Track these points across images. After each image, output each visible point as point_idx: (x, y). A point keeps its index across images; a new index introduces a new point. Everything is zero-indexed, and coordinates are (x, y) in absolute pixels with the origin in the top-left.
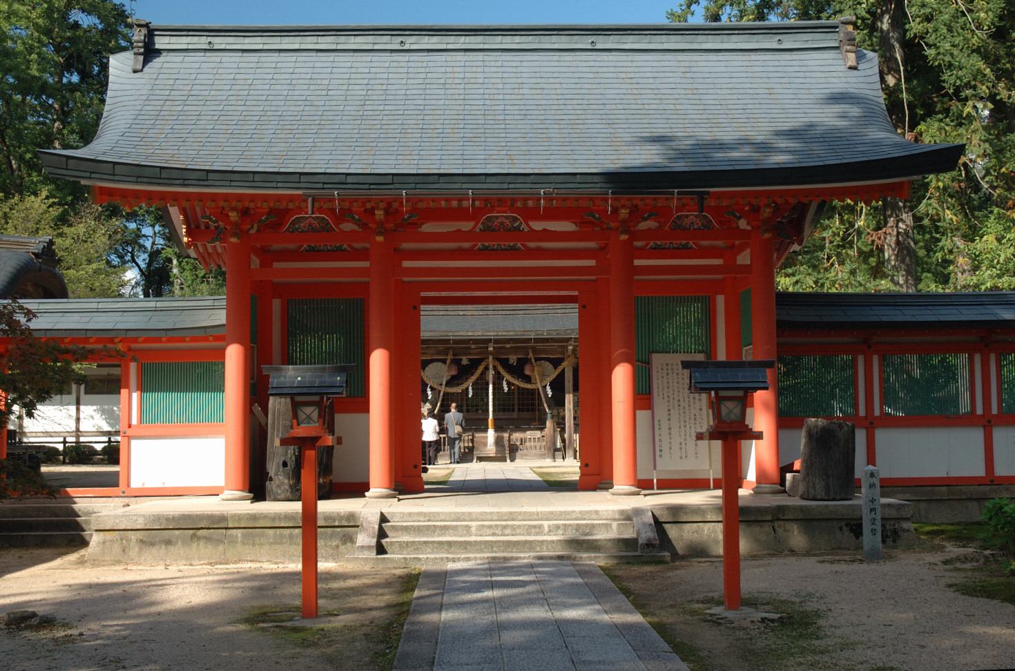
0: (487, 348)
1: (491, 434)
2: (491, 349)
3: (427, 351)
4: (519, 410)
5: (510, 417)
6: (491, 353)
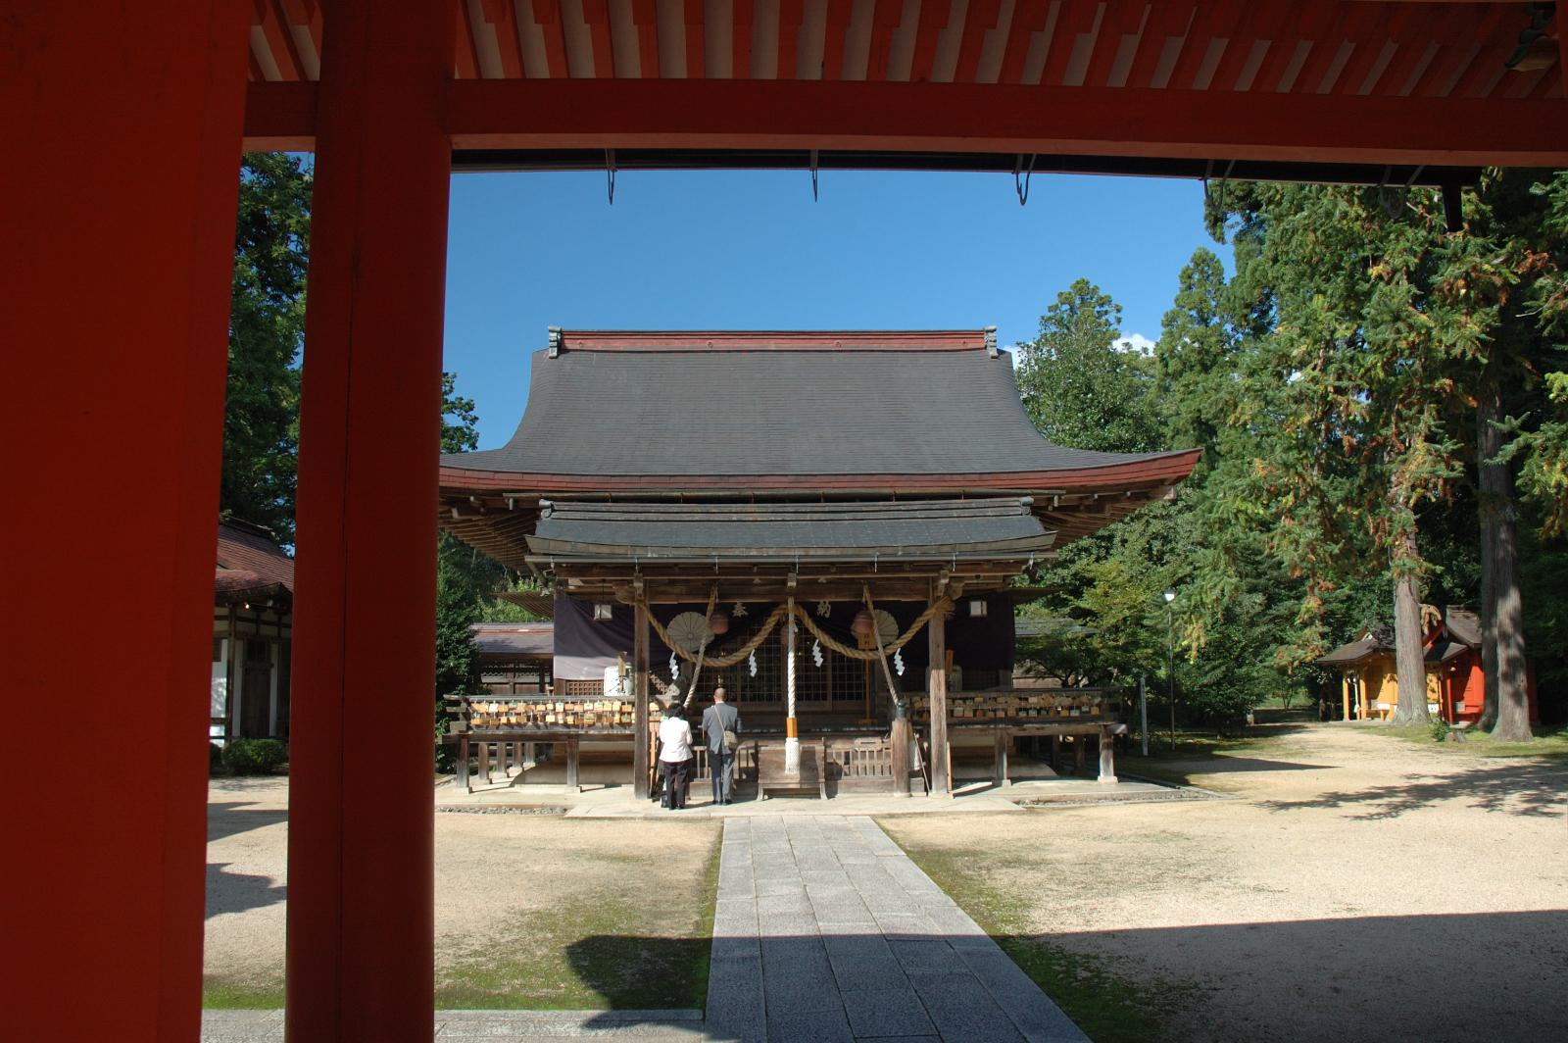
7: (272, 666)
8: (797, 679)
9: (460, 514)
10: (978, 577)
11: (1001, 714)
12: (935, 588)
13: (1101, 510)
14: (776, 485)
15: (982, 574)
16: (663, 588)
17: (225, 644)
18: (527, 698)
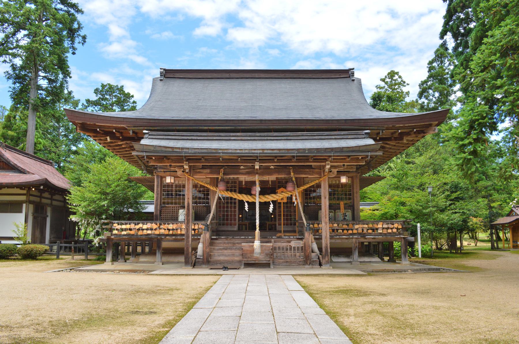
0: (253, 167)
1: (257, 244)
2: (257, 167)
7: (47, 216)
8: (255, 219)
9: (111, 139)
10: (344, 165)
11: (355, 231)
12: (324, 171)
13: (402, 139)
14: (251, 125)
15: (345, 164)
16: (199, 170)
17: (24, 205)
18: (135, 222)
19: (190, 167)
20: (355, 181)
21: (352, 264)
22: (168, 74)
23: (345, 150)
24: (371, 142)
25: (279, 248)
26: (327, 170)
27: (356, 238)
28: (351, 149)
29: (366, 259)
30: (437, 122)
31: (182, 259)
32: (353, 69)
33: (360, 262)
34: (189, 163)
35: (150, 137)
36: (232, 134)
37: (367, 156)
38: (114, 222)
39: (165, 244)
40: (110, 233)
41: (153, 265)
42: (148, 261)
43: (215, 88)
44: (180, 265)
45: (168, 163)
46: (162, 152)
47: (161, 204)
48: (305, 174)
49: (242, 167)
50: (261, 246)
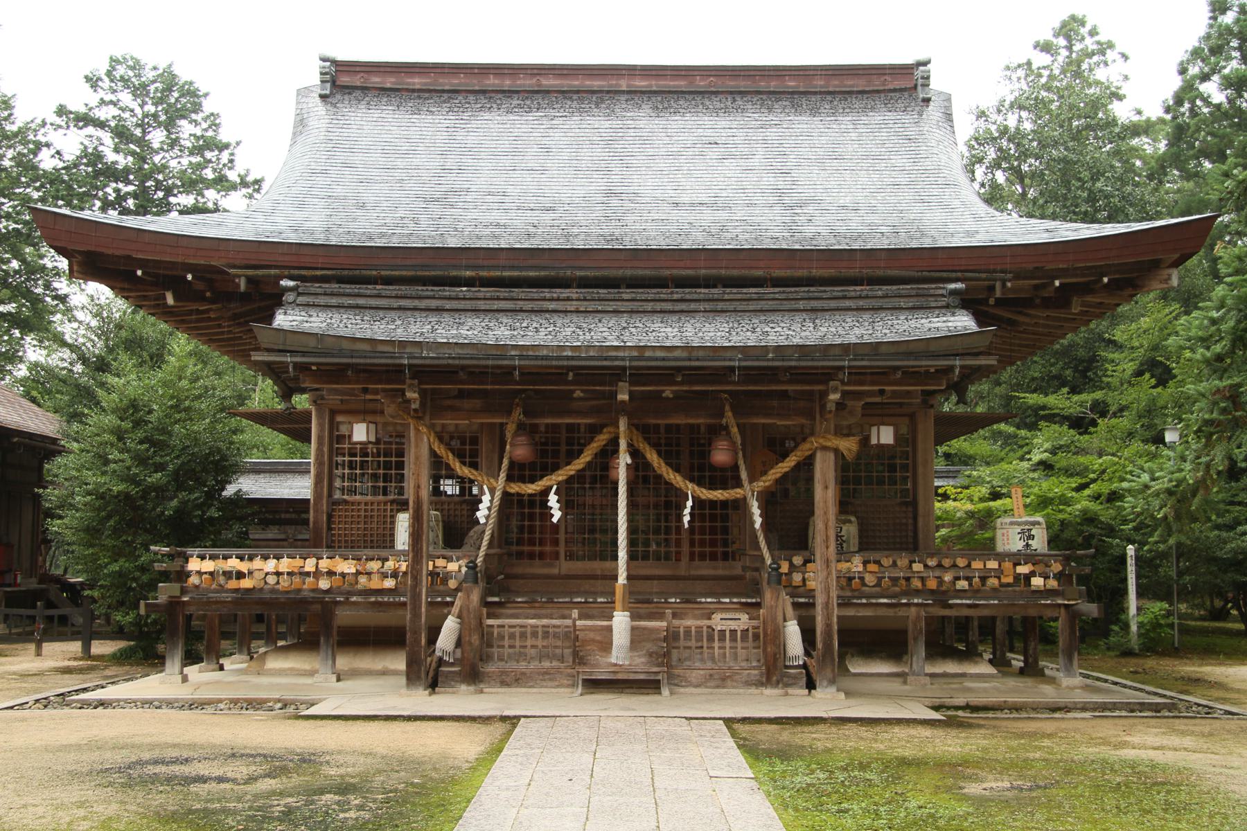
0: (613, 395)
1: (621, 621)
2: (623, 397)
3: (457, 403)
4: (692, 558)
5: (727, 573)
6: (623, 408)
9: (176, 298)
10: (882, 392)
12: (823, 407)
13: (1067, 304)
16: (448, 402)
19: (423, 393)
20: (920, 427)
21: (905, 683)
22: (348, 82)
23: (883, 349)
24: (963, 322)
25: (688, 632)
26: (831, 406)
27: (917, 605)
28: (902, 349)
29: (951, 667)
30: (1176, 256)
31: (398, 662)
32: (928, 62)
33: (932, 675)
34: (420, 383)
35: (301, 299)
36: (547, 293)
37: (951, 369)
38: (190, 551)
39: (344, 617)
40: (177, 586)
41: (308, 681)
42: (291, 669)
43: (494, 128)
44: (391, 680)
45: (357, 382)
46: (341, 352)
47: (330, 495)
48: (767, 415)
49: (578, 394)
50: (633, 629)
